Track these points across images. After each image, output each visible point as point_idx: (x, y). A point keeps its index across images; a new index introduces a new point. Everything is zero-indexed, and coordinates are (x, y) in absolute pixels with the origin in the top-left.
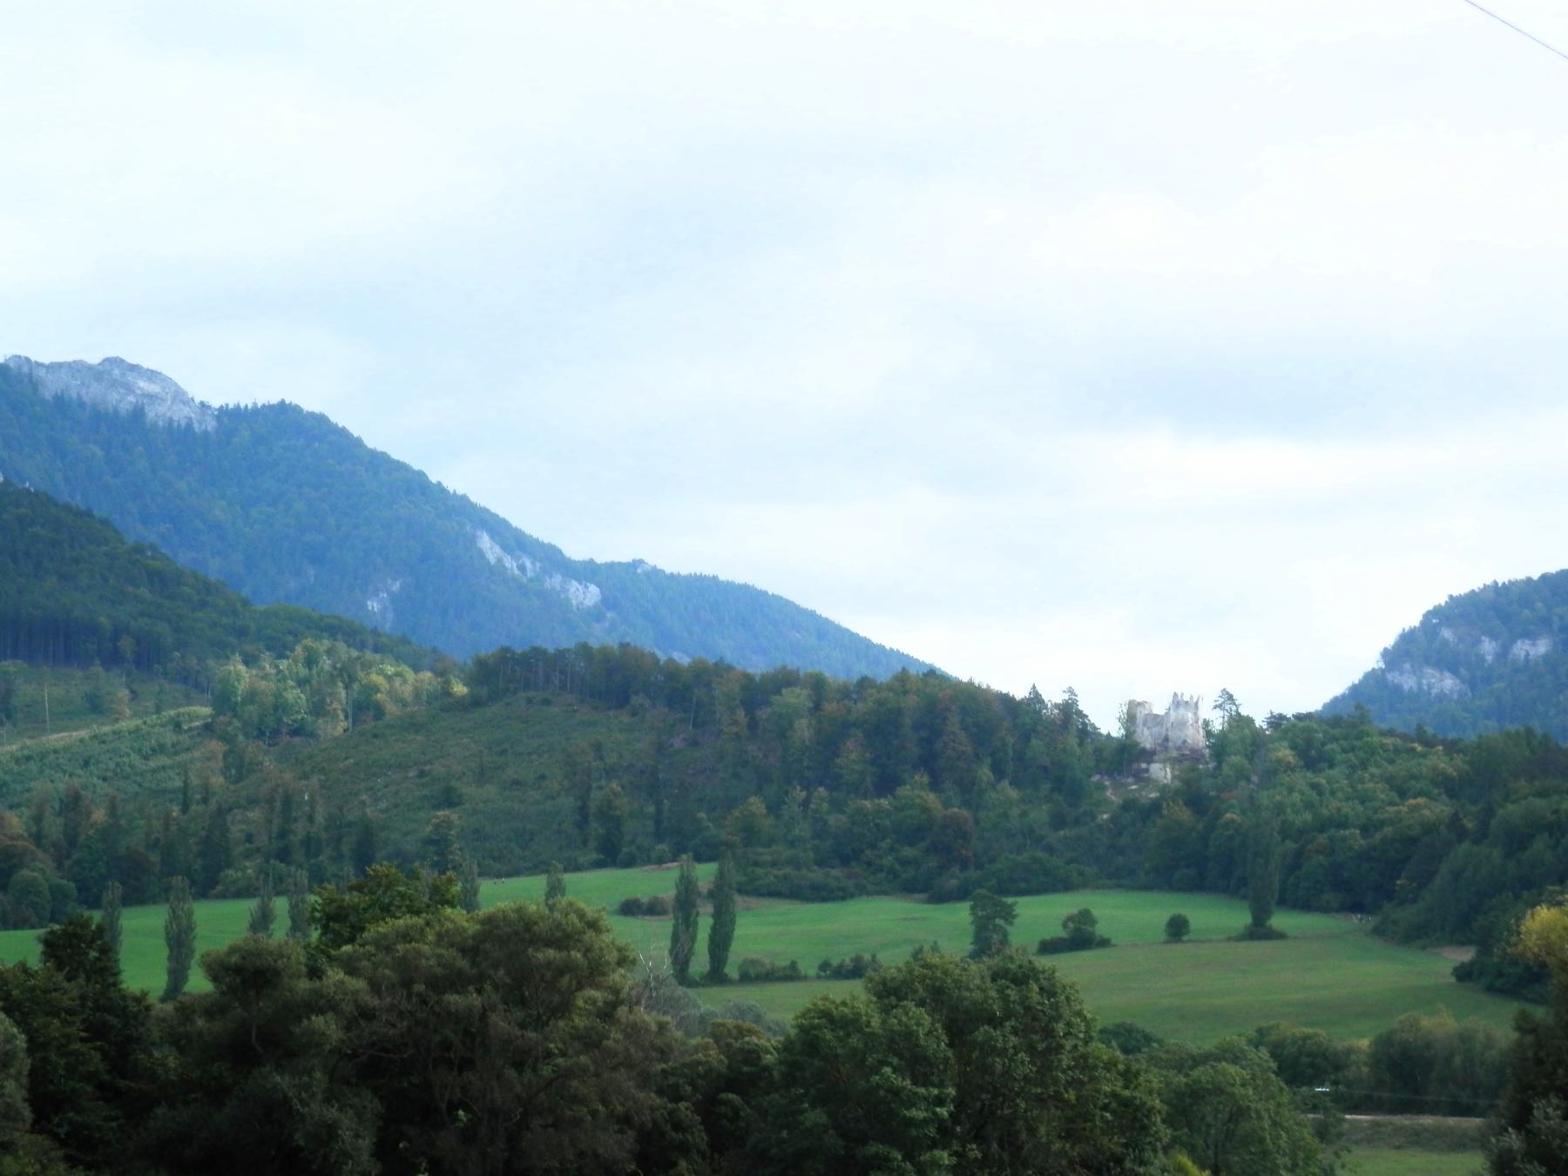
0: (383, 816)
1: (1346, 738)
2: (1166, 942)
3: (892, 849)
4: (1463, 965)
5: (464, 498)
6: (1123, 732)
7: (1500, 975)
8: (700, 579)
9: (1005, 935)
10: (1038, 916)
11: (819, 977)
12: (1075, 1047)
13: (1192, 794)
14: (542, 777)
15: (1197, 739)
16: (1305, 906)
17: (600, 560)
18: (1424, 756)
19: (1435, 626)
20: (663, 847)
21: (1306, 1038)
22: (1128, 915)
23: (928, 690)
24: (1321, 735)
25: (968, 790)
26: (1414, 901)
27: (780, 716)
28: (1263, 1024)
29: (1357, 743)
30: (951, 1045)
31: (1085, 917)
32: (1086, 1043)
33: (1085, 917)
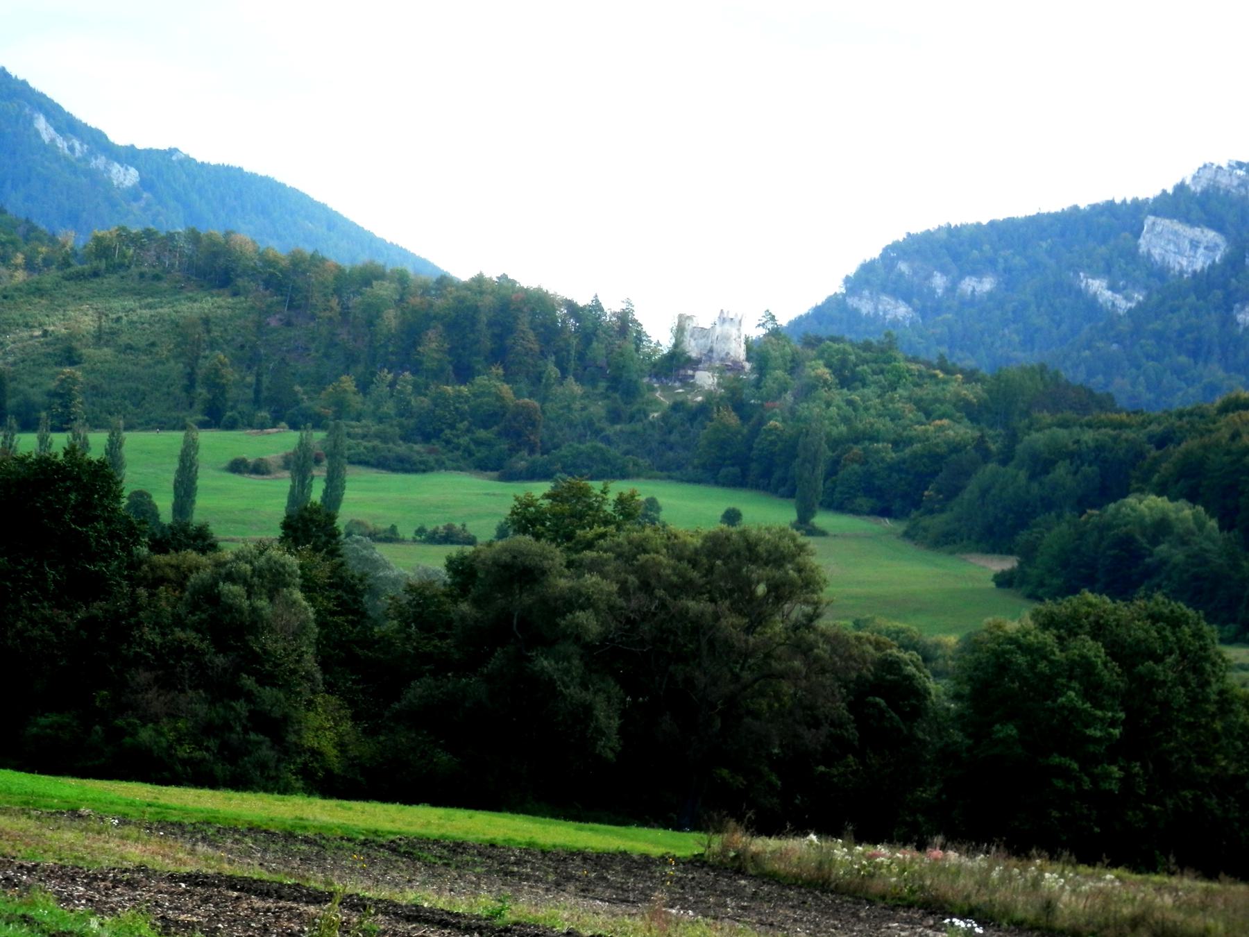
0: (12, 369)
1: (875, 361)
3: (468, 431)
4: (1003, 573)
5: (24, 83)
7: (1041, 584)
8: (228, 169)
11: (415, 541)
13: (735, 399)
14: (153, 344)
15: (738, 352)
17: (139, 146)
19: (892, 259)
20: (264, 414)
24: (853, 358)
26: (942, 511)
27: (369, 305)
29: (888, 367)
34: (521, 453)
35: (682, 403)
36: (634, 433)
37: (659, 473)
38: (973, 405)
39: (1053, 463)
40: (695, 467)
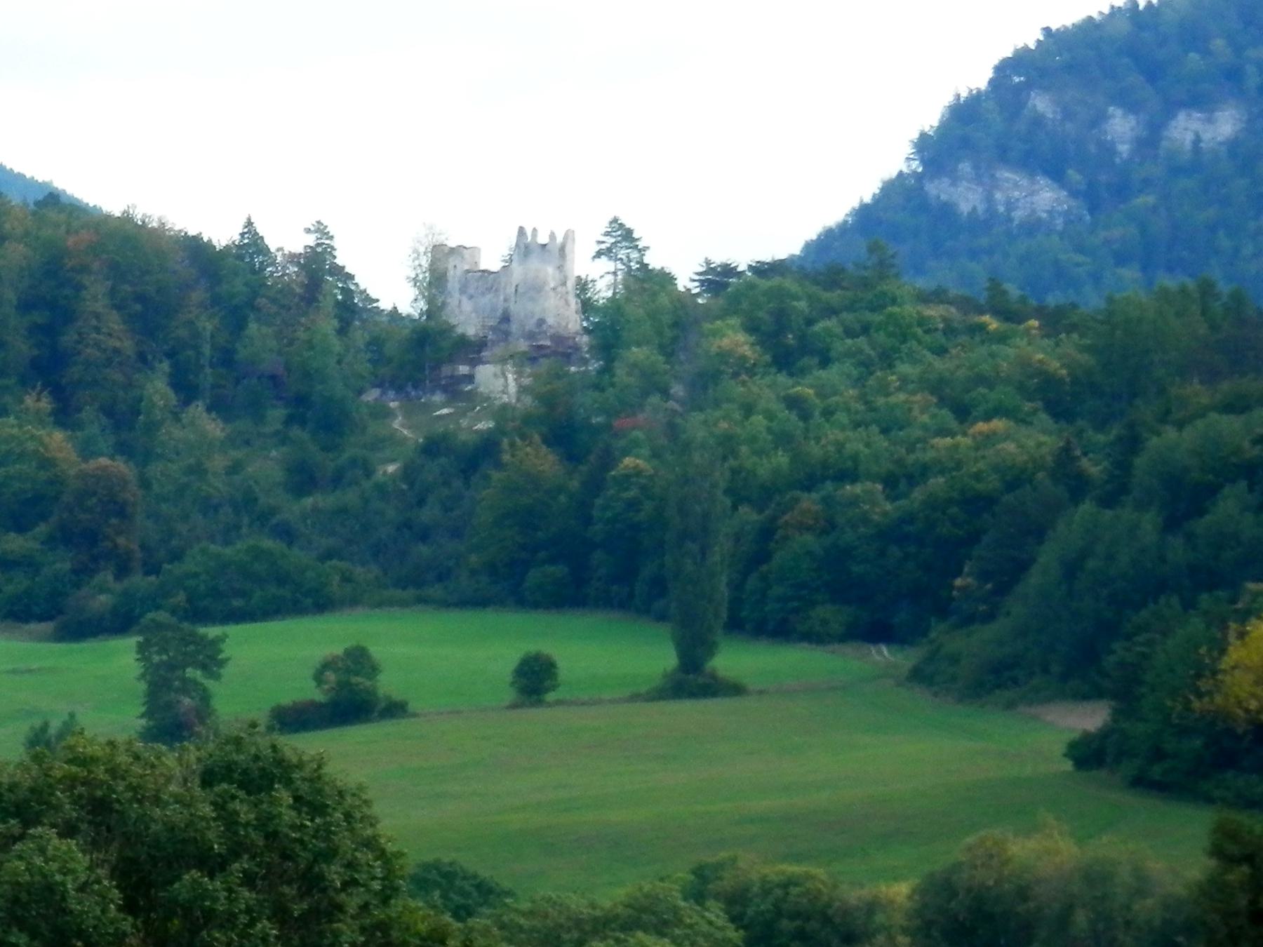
1: (851, 308)
2: (514, 706)
6: (422, 305)
7: (1158, 754)
9: (205, 697)
10: (264, 664)
12: (365, 907)
13: (561, 429)
15: (566, 317)
16: (779, 629)
18: (1002, 338)
19: (1018, 89)
21: (787, 884)
22: (436, 654)
23: (47, 233)
24: (802, 305)
25: (125, 421)
26: (989, 617)
28: (709, 858)
30: (129, 907)
31: (358, 659)
32: (385, 898)
33: (358, 659)
34: (98, 579)
35: (445, 437)
36: (343, 511)
37: (399, 593)
38: (1061, 381)
39: (1212, 491)
40: (474, 573)
